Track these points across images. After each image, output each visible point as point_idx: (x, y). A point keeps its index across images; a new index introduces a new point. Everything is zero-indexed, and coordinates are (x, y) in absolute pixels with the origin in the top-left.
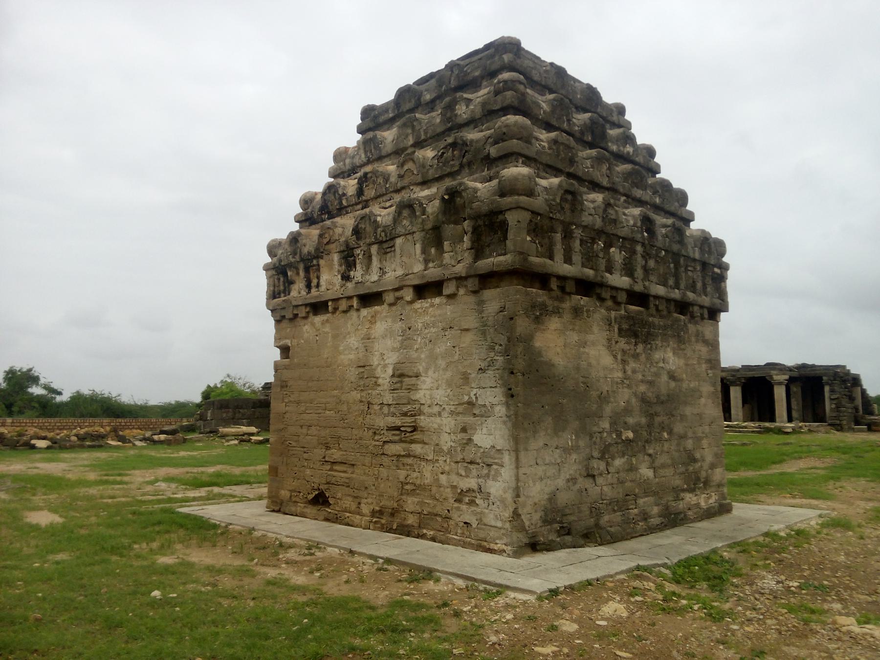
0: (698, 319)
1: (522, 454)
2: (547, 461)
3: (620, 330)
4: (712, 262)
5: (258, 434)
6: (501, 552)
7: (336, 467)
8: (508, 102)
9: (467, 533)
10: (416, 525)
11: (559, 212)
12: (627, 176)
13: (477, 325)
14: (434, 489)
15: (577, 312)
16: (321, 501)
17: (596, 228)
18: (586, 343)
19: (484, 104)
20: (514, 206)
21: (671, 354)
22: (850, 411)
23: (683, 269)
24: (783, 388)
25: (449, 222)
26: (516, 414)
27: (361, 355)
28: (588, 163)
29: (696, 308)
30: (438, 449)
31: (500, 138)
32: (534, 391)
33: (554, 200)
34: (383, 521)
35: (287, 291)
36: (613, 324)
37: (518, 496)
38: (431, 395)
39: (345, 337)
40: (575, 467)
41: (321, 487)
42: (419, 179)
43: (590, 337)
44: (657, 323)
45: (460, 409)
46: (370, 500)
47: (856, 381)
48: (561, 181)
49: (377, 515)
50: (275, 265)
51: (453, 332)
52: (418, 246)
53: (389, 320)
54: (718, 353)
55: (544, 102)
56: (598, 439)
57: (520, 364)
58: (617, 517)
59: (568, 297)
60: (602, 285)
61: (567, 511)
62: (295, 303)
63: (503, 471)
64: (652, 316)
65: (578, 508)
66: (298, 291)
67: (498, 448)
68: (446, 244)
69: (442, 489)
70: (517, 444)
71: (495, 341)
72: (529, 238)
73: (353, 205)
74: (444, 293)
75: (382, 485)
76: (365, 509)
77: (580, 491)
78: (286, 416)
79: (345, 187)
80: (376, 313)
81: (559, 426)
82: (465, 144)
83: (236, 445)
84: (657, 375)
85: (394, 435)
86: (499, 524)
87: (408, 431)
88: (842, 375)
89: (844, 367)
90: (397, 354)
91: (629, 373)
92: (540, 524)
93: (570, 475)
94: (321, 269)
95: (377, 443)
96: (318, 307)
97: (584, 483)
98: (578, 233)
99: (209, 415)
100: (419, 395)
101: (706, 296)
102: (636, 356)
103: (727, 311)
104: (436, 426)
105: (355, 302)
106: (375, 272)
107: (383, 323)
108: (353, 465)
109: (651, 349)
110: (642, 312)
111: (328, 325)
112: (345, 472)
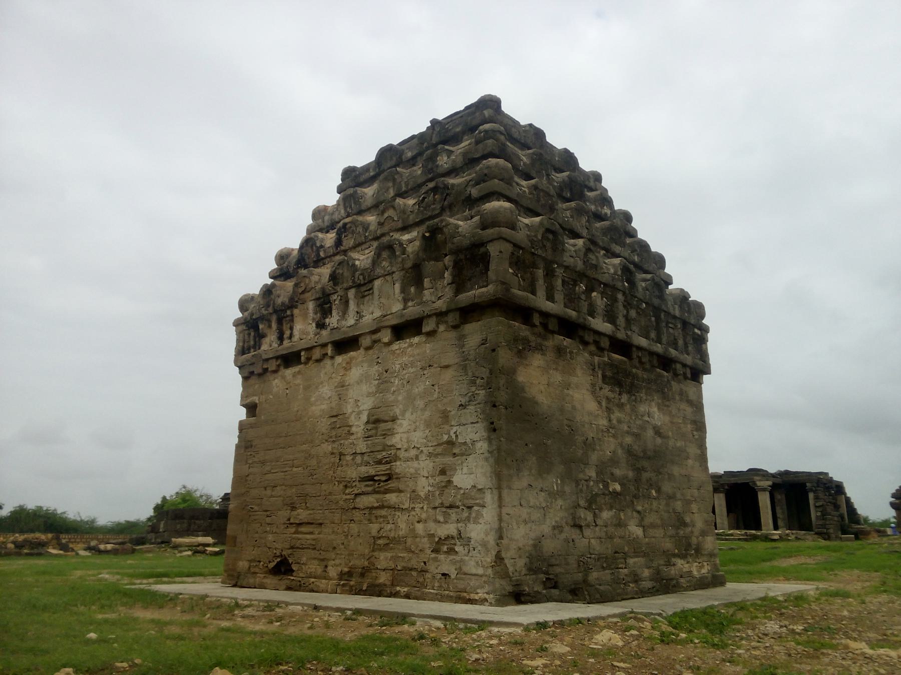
0: (681, 377)
1: (505, 492)
2: (531, 504)
3: (604, 376)
4: (693, 321)
5: (214, 545)
6: (483, 601)
7: (303, 529)
8: (489, 149)
9: (445, 586)
10: (388, 583)
11: (541, 248)
12: (606, 231)
13: (457, 360)
14: (409, 540)
15: (560, 351)
16: (283, 570)
17: (578, 269)
18: (569, 385)
19: (465, 154)
20: (496, 236)
21: (656, 409)
22: (836, 519)
23: (664, 324)
24: (768, 494)
25: (430, 259)
26: (499, 449)
27: (334, 405)
28: (568, 213)
29: (678, 366)
30: (415, 496)
31: (483, 178)
32: (519, 431)
33: (536, 236)
34: (352, 583)
35: (257, 345)
36: (597, 369)
37: (501, 538)
38: (408, 438)
39: (317, 388)
40: (561, 514)
41: (284, 553)
42: (400, 225)
43: (574, 380)
44: (640, 375)
45: (439, 450)
46: (337, 562)
47: (839, 488)
48: (542, 219)
49: (346, 577)
50: (246, 319)
51: (432, 370)
52: (397, 286)
53: (365, 365)
54: (703, 416)
55: (524, 157)
56: (585, 487)
57: (503, 396)
58: (606, 575)
59: (551, 336)
60: (586, 328)
61: (553, 561)
62: (265, 357)
63: (484, 511)
64: (636, 367)
65: (565, 559)
66: (269, 345)
67: (480, 487)
68: (427, 282)
69: (418, 539)
70: (500, 482)
71: (477, 375)
72: (511, 271)
73: (330, 257)
74: (424, 330)
75: (352, 543)
76: (333, 572)
77: (567, 541)
78: (250, 478)
79: (322, 240)
80: (351, 359)
81: (544, 468)
82: (446, 187)
83: (189, 556)
84: (643, 428)
85: (367, 486)
86: (480, 571)
87: (383, 480)
88: (825, 481)
89: (827, 474)
90: (373, 399)
91: (614, 422)
92: (524, 571)
93: (556, 522)
94: (295, 319)
95: (348, 497)
96: (290, 359)
97: (569, 533)
98: (559, 272)
99: (162, 526)
100: (396, 440)
101: (688, 354)
102: (621, 406)
103: (709, 373)
104: (412, 471)
105: (329, 350)
106: (351, 316)
107: (358, 369)
108: (321, 524)
109: (635, 400)
110: (625, 362)
111: (299, 376)
112: (311, 533)
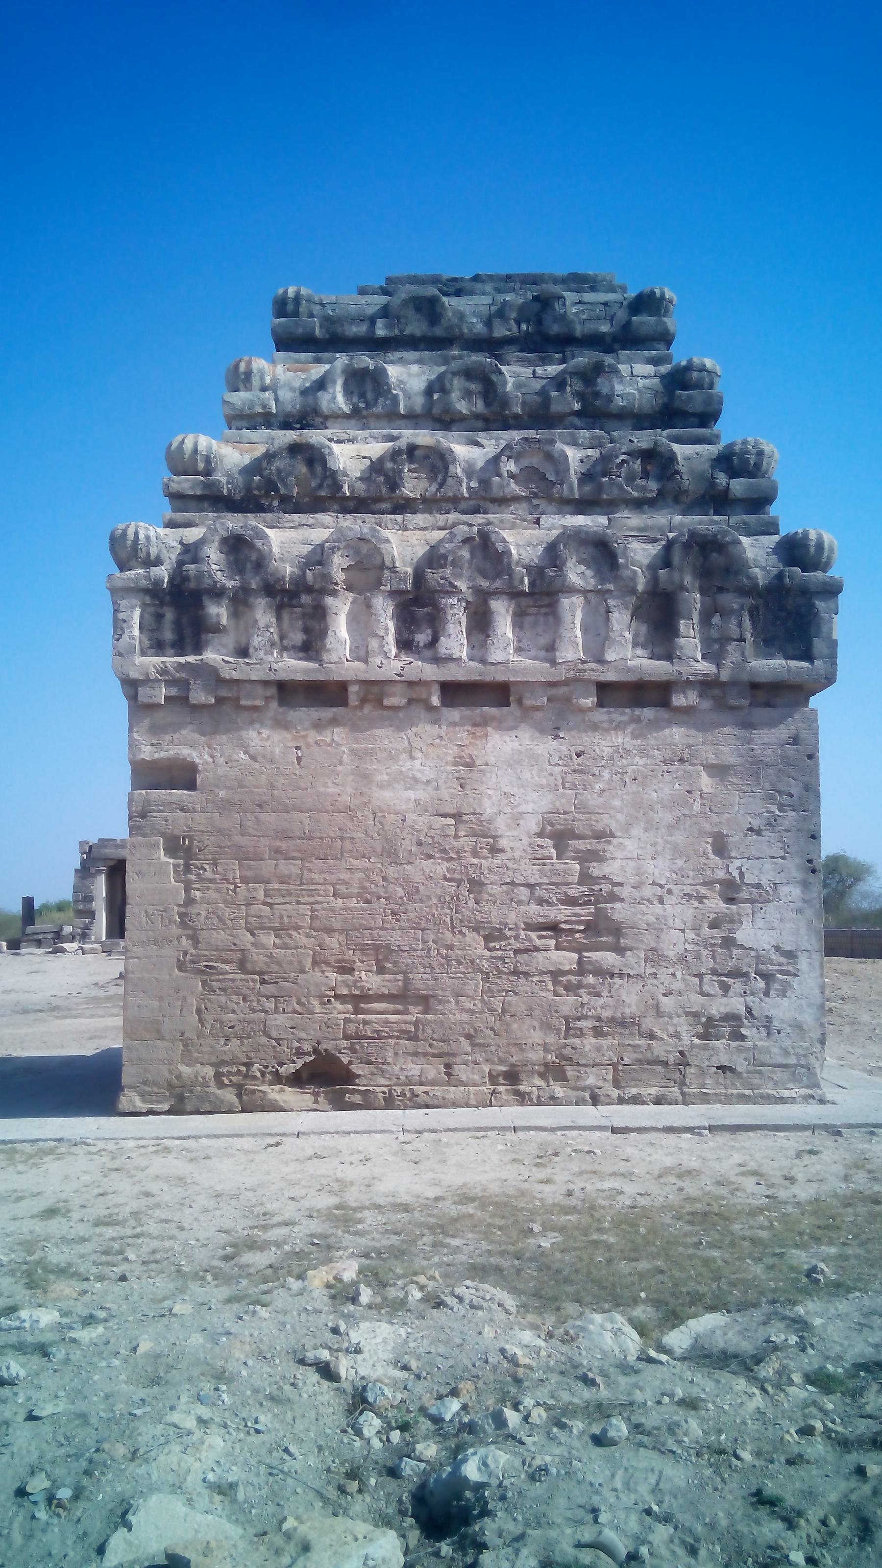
30: (655, 956)
90: (550, 797)
